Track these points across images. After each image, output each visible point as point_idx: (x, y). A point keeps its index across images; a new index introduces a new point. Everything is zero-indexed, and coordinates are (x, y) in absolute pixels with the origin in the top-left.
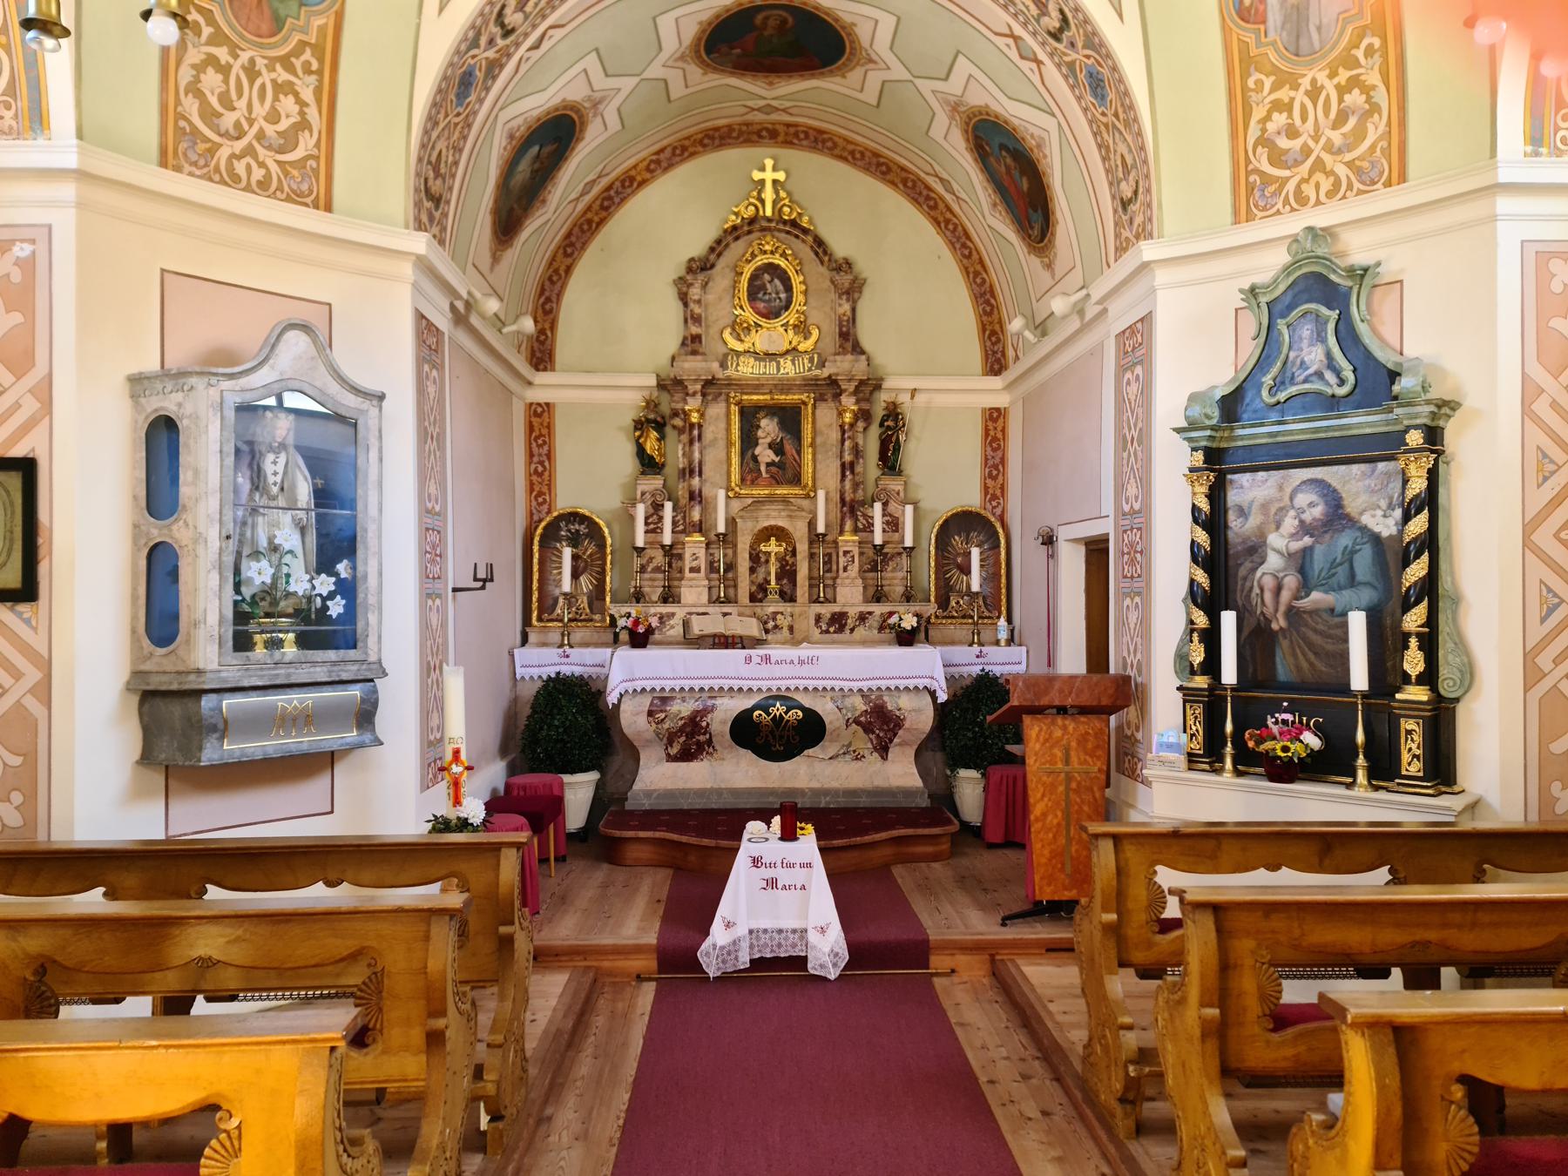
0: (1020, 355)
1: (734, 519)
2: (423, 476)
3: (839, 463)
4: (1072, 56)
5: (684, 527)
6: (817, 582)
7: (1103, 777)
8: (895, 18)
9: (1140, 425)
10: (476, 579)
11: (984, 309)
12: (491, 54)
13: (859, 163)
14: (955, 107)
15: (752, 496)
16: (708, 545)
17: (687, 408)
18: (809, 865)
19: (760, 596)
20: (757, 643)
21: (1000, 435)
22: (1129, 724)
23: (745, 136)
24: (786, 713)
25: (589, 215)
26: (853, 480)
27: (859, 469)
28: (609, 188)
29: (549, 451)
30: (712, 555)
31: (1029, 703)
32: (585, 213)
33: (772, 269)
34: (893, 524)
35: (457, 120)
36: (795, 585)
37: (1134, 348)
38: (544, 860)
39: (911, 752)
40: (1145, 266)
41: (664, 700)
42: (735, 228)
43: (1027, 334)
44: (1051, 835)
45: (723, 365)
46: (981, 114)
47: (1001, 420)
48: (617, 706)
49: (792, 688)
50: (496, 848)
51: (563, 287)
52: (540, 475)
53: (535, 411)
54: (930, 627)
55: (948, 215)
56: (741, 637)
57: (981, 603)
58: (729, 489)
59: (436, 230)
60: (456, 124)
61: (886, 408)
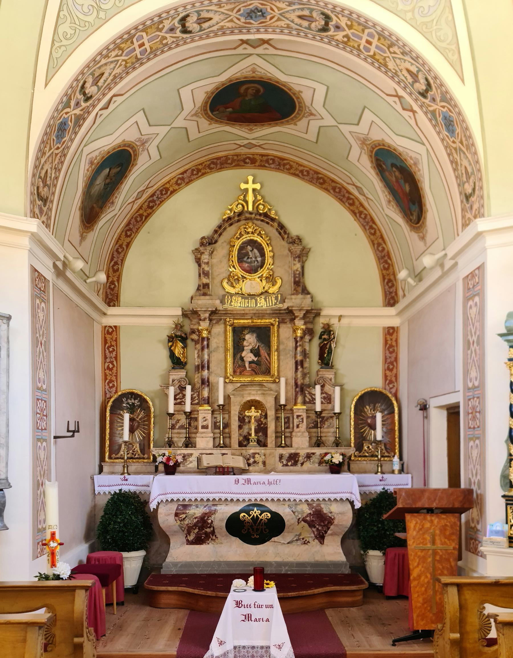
0: (406, 293)
1: (229, 396)
2: (35, 366)
3: (294, 361)
4: (434, 107)
5: (197, 401)
6: (280, 435)
7: (456, 552)
8: (326, 87)
9: (478, 333)
10: (68, 431)
11: (383, 266)
12: (78, 111)
13: (306, 178)
14: (363, 142)
15: (240, 382)
16: (213, 412)
17: (200, 328)
18: (271, 606)
19: (245, 443)
20: (243, 471)
21: (394, 344)
22: (473, 519)
23: (236, 163)
24: (260, 515)
25: (141, 212)
26: (302, 371)
27: (306, 365)
28: (153, 195)
29: (116, 355)
30: (215, 418)
31: (409, 506)
32: (139, 210)
33: (252, 243)
34: (328, 399)
35: (57, 152)
36: (266, 436)
37: (474, 286)
38: (109, 604)
39: (339, 539)
40: (479, 235)
41: (185, 507)
42: (229, 218)
43: (410, 280)
44: (423, 589)
45: (222, 302)
46: (379, 145)
47: (395, 334)
48: (156, 510)
49: (264, 499)
50: (73, 589)
51: (125, 256)
52: (111, 370)
53: (108, 331)
54: (351, 462)
55: (361, 209)
56: (233, 468)
57: (383, 447)
58: (226, 377)
59: (44, 218)
60: (57, 155)
61: (323, 328)
